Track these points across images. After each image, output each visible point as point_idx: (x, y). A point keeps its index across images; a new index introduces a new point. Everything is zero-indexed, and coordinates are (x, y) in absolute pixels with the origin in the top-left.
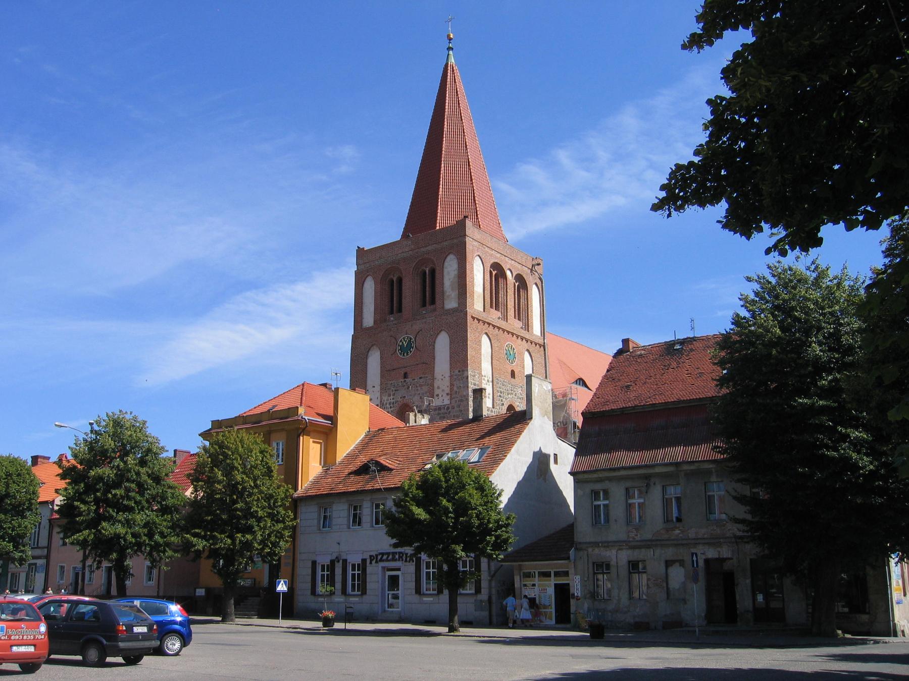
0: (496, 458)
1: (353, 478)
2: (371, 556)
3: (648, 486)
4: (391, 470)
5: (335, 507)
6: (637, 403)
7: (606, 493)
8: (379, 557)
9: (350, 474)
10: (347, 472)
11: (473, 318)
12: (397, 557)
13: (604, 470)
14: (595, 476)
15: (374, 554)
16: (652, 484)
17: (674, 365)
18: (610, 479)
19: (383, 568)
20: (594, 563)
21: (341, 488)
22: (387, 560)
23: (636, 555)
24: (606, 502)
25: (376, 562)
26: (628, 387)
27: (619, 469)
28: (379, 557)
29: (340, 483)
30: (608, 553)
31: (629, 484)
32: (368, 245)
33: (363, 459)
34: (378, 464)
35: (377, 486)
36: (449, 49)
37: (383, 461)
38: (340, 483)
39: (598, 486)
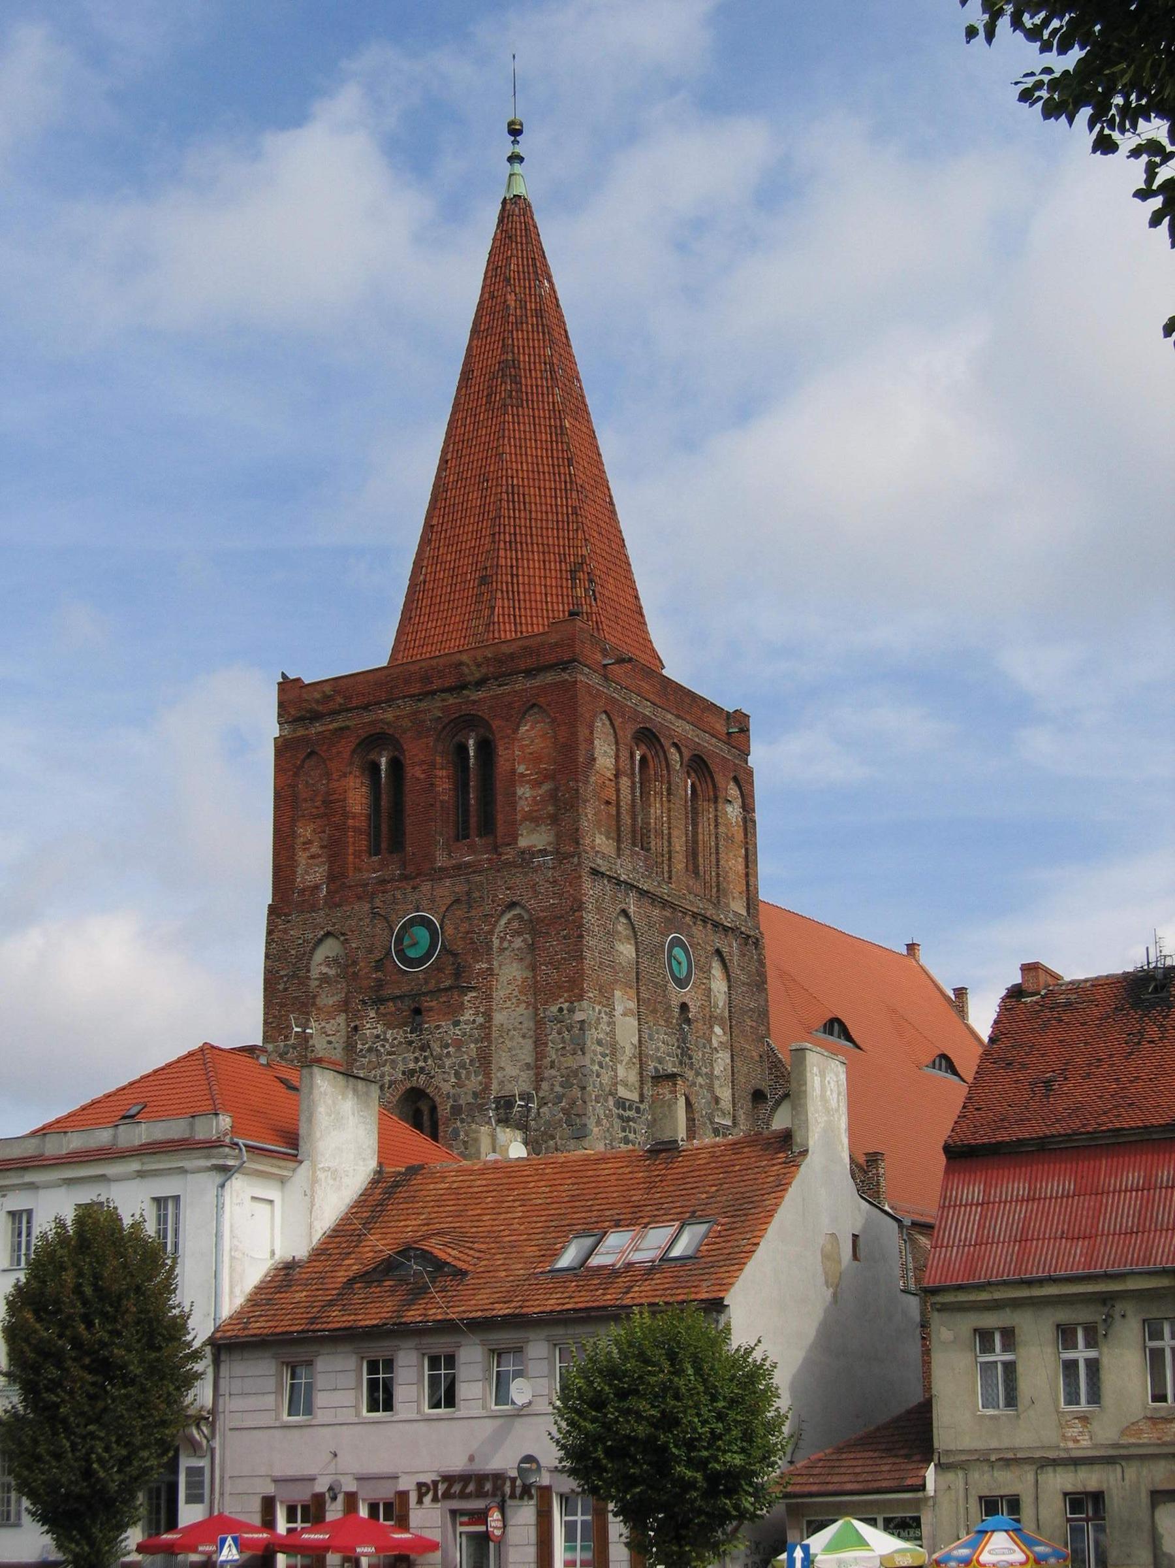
0: (729, 1252)
1: (360, 1293)
2: (420, 1485)
3: (1108, 1320)
4: (463, 1273)
5: (321, 1364)
6: (1075, 1124)
7: (1009, 1335)
8: (441, 1488)
9: (352, 1281)
10: (342, 1276)
11: (595, 872)
12: (488, 1487)
13: (1005, 1283)
14: (984, 1296)
15: (427, 1478)
16: (1117, 1317)
17: (1153, 1032)
18: (1016, 1304)
19: (454, 1513)
20: (981, 1498)
21: (338, 1319)
22: (463, 1496)
23: (1089, 1479)
24: (1008, 1357)
25: (435, 1499)
26: (1048, 1083)
27: (1041, 1282)
28: (441, 1488)
29: (331, 1303)
30: (76, 1506)
31: (1063, 1315)
32: (315, 670)
33: (379, 1245)
34: (426, 1257)
35: (436, 1314)
36: (515, 158)
37: (435, 1247)
38: (331, 1303)
39: (989, 1320)
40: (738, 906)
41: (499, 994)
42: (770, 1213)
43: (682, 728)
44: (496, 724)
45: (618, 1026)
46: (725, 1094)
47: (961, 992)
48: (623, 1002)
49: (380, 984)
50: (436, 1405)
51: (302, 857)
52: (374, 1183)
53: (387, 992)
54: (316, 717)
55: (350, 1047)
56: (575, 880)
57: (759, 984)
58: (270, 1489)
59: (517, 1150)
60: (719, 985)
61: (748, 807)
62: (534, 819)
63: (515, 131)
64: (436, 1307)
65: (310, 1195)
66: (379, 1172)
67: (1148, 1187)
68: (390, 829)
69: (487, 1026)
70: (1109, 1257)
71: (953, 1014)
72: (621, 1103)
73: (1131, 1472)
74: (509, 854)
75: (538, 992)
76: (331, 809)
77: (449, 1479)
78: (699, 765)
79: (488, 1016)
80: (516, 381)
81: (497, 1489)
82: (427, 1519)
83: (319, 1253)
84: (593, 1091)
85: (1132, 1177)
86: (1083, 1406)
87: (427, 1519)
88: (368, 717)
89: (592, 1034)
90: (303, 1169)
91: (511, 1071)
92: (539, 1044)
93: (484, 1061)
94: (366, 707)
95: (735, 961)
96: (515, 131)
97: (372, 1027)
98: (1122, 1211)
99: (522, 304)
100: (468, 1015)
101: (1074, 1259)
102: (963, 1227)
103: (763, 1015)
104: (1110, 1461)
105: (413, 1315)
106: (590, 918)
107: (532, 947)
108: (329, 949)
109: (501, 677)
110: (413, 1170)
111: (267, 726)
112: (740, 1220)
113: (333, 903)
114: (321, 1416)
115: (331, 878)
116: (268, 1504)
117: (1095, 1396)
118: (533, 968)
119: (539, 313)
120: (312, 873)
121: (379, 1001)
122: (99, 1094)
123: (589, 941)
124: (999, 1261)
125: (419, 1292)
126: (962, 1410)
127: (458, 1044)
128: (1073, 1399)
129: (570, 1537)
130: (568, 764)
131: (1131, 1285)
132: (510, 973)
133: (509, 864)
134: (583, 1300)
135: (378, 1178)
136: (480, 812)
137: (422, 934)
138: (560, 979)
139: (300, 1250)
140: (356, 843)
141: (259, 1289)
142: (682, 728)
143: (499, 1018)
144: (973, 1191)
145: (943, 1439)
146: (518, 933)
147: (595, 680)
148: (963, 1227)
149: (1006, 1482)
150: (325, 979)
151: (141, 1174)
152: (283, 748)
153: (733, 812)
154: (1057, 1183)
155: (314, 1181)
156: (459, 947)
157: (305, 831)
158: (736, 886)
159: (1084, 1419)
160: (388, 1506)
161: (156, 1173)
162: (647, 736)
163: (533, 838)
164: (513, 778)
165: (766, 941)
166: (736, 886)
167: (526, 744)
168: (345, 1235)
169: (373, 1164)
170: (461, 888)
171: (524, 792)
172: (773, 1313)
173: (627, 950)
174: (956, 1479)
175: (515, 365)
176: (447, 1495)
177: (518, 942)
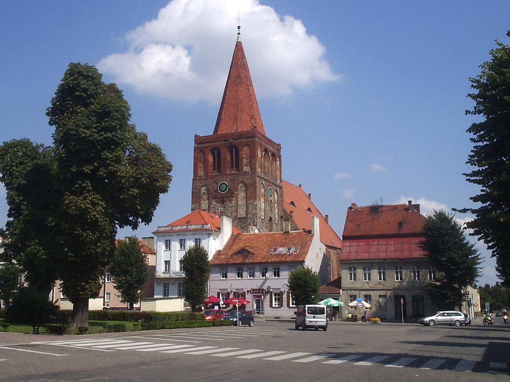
1: (235, 257)
3: (372, 267)
6: (365, 233)
17: (376, 217)
18: (356, 263)
21: (231, 261)
22: (256, 293)
31: (364, 265)
33: (236, 248)
35: (251, 261)
37: (247, 248)
39: (351, 266)
40: (279, 181)
41: (239, 198)
42: (310, 245)
43: (271, 148)
44: (239, 147)
45: (261, 204)
46: (277, 217)
47: (310, 195)
48: (262, 200)
49: (216, 195)
50: (238, 277)
51: (199, 170)
52: (232, 236)
53: (217, 196)
54: (202, 143)
55: (209, 207)
56: (255, 178)
57: (282, 196)
58: (219, 291)
59: (256, 231)
60: (276, 196)
61: (280, 162)
62: (246, 165)
63: (239, 28)
64: (249, 260)
65: (222, 238)
66: (232, 234)
67: (378, 245)
68: (218, 165)
69: (237, 204)
70: (372, 256)
71: (308, 199)
72: (262, 219)
73: (376, 292)
74: (241, 172)
75: (247, 198)
76: (205, 161)
77: (253, 290)
78: (273, 155)
79: (237, 202)
80: (240, 79)
81: (262, 292)
82: (249, 297)
83: (224, 249)
84: (258, 217)
85: (375, 243)
86: (367, 281)
87: (249, 297)
88: (213, 144)
89: (258, 206)
90: (221, 234)
91: (242, 213)
92: (247, 208)
93: (236, 211)
94: (213, 142)
95: (278, 192)
96: (239, 28)
97: (214, 203)
98: (374, 249)
99: (241, 64)
100: (233, 202)
101: (366, 256)
102: (346, 250)
103: (283, 201)
104: (372, 290)
105: (247, 261)
106: (257, 185)
107: (246, 190)
108: (204, 188)
109: (240, 138)
110: (239, 234)
111: (192, 144)
112: (305, 246)
113: (206, 179)
114: (228, 278)
115: (205, 174)
116: (218, 293)
117: (369, 279)
118: (246, 194)
119: (244, 65)
120: (201, 173)
121: (215, 198)
122: (179, 219)
123: (257, 189)
124: (353, 256)
125: (246, 257)
126: (346, 281)
127: (231, 207)
128: (365, 279)
129: (275, 300)
130: (252, 156)
131: (377, 261)
132: (242, 195)
133: (242, 174)
134: (279, 260)
135: (232, 235)
136: (237, 164)
137: (225, 186)
138: (251, 195)
139: (221, 248)
140: (211, 168)
141: (214, 255)
142: (271, 148)
143: (239, 203)
144: (348, 244)
145: (343, 285)
146: (243, 187)
147: (258, 140)
148: (346, 250)
149: (354, 293)
150: (204, 193)
151: (193, 234)
152: (195, 149)
153: (278, 163)
154: (362, 243)
155: (223, 236)
156: (232, 189)
157: (200, 165)
158: (279, 177)
159: (367, 283)
160: (242, 294)
161: (195, 234)
162: (266, 150)
163: (246, 169)
164: (242, 158)
165: (283, 188)
166: (279, 177)
167: (245, 151)
168: (229, 246)
169: (231, 233)
170: (232, 178)
171: (245, 160)
172: (313, 262)
173: (263, 190)
174: (345, 292)
175: (240, 76)
176: (253, 293)
177: (243, 189)
